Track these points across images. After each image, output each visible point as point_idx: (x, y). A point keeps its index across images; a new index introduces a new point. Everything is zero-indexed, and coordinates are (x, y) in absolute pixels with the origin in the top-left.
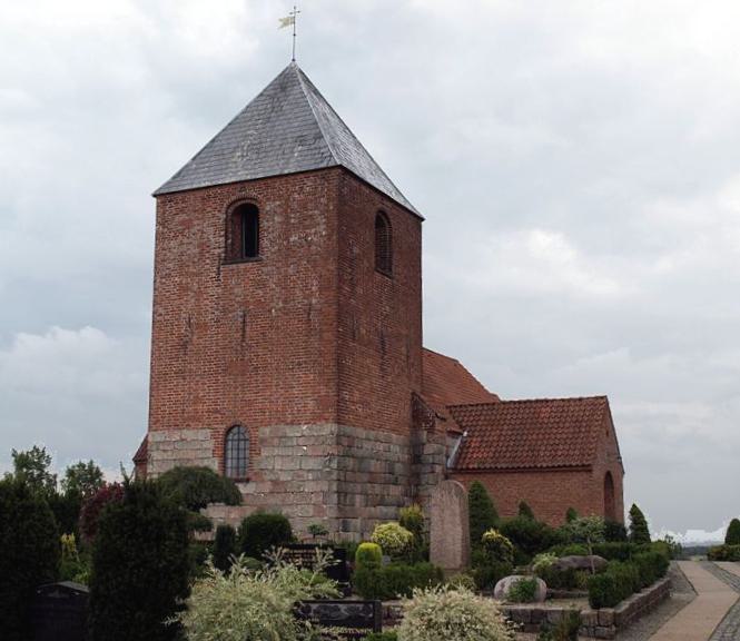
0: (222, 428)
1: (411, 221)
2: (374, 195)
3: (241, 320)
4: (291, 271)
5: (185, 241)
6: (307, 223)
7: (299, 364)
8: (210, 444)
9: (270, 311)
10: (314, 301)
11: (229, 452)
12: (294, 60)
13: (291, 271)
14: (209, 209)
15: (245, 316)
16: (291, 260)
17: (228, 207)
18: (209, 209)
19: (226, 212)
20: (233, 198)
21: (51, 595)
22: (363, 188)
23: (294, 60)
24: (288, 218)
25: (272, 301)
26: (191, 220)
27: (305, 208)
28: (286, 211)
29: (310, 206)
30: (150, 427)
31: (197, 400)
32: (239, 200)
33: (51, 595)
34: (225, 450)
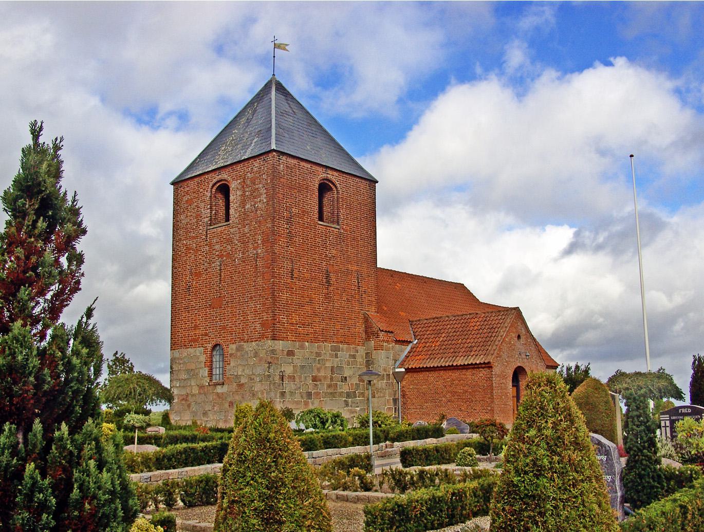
0: (209, 346)
1: (363, 185)
2: (315, 168)
3: (218, 268)
4: (246, 230)
5: (189, 214)
6: (255, 194)
7: (251, 298)
8: (203, 358)
9: (235, 260)
10: (259, 251)
11: (214, 370)
12: (274, 75)
13: (246, 230)
14: (201, 190)
15: (221, 265)
16: (246, 222)
17: (212, 188)
18: (201, 190)
19: (211, 191)
20: (215, 181)
21: (75, 401)
22: (302, 164)
23: (274, 75)
24: (244, 192)
25: (236, 254)
26: (191, 199)
27: (254, 184)
28: (243, 187)
29: (257, 181)
30: (171, 347)
31: (196, 327)
32: (218, 182)
33: (75, 401)
34: (212, 361)
